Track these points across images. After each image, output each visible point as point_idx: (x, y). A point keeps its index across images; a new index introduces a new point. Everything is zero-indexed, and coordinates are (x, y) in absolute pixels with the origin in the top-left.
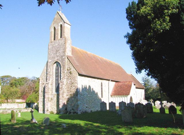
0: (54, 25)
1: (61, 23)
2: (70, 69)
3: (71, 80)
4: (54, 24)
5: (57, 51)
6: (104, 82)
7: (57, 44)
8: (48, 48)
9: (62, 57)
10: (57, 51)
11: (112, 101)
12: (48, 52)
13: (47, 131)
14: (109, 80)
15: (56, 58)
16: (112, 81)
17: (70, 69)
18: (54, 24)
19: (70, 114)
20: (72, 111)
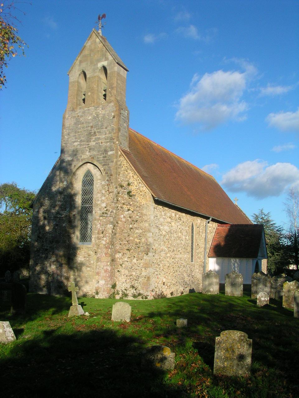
0: (84, 66)
1: (105, 63)
2: (129, 185)
3: (130, 212)
4: (81, 62)
5: (90, 135)
6: (199, 220)
7: (90, 118)
8: (63, 125)
9: (106, 151)
10: (90, 135)
11: (193, 289)
12: (63, 136)
13: (287, 268)
14: (207, 218)
15: (88, 153)
16: (213, 220)
17: (129, 185)
18: (81, 62)
19: (9, 332)
20: (131, 292)
